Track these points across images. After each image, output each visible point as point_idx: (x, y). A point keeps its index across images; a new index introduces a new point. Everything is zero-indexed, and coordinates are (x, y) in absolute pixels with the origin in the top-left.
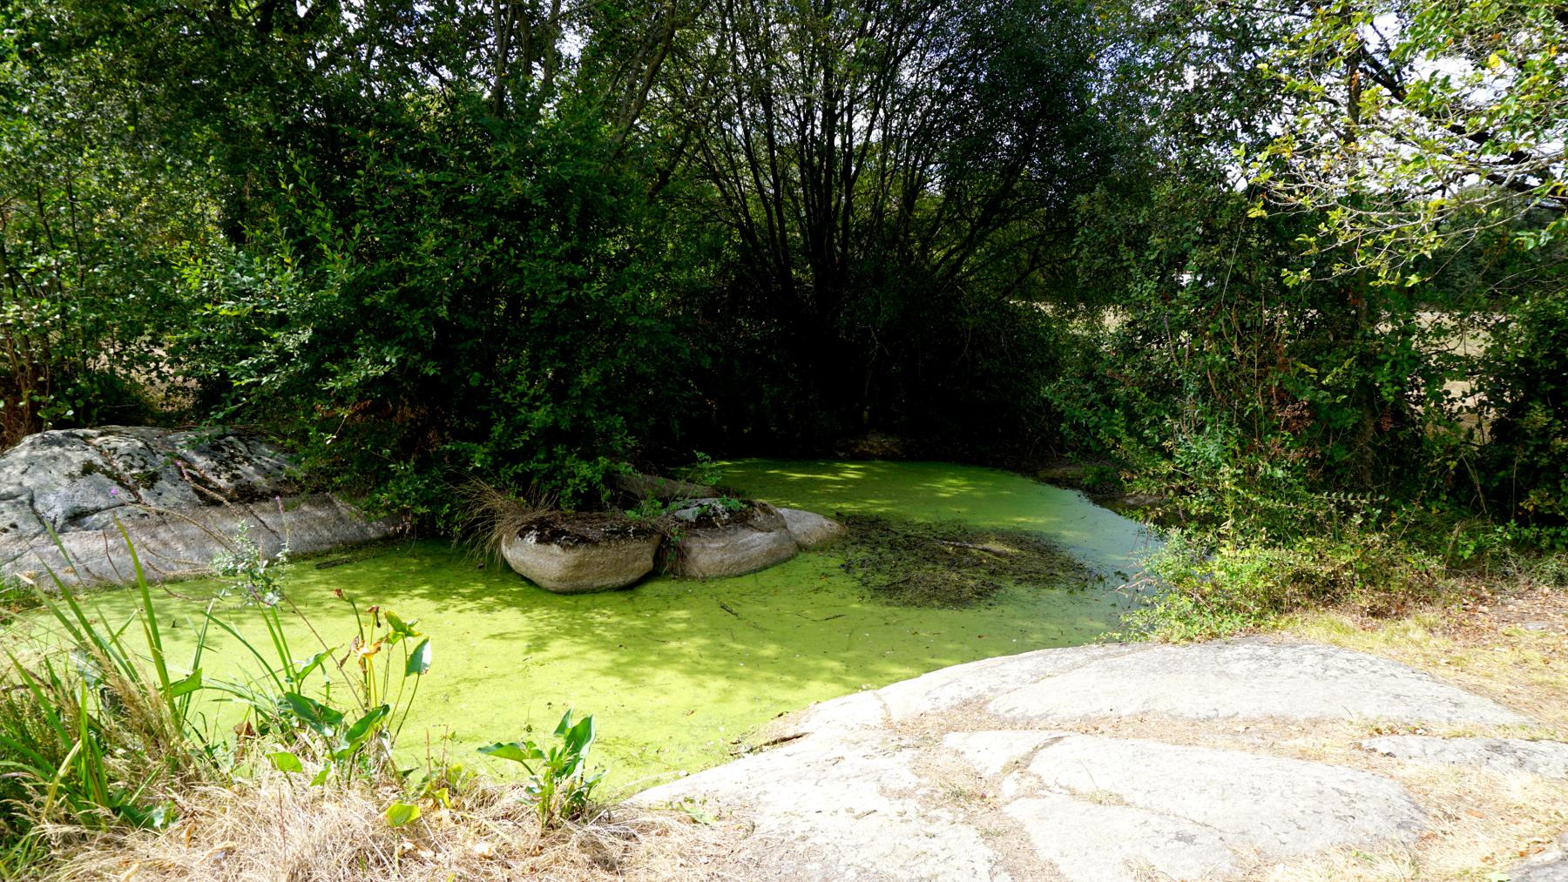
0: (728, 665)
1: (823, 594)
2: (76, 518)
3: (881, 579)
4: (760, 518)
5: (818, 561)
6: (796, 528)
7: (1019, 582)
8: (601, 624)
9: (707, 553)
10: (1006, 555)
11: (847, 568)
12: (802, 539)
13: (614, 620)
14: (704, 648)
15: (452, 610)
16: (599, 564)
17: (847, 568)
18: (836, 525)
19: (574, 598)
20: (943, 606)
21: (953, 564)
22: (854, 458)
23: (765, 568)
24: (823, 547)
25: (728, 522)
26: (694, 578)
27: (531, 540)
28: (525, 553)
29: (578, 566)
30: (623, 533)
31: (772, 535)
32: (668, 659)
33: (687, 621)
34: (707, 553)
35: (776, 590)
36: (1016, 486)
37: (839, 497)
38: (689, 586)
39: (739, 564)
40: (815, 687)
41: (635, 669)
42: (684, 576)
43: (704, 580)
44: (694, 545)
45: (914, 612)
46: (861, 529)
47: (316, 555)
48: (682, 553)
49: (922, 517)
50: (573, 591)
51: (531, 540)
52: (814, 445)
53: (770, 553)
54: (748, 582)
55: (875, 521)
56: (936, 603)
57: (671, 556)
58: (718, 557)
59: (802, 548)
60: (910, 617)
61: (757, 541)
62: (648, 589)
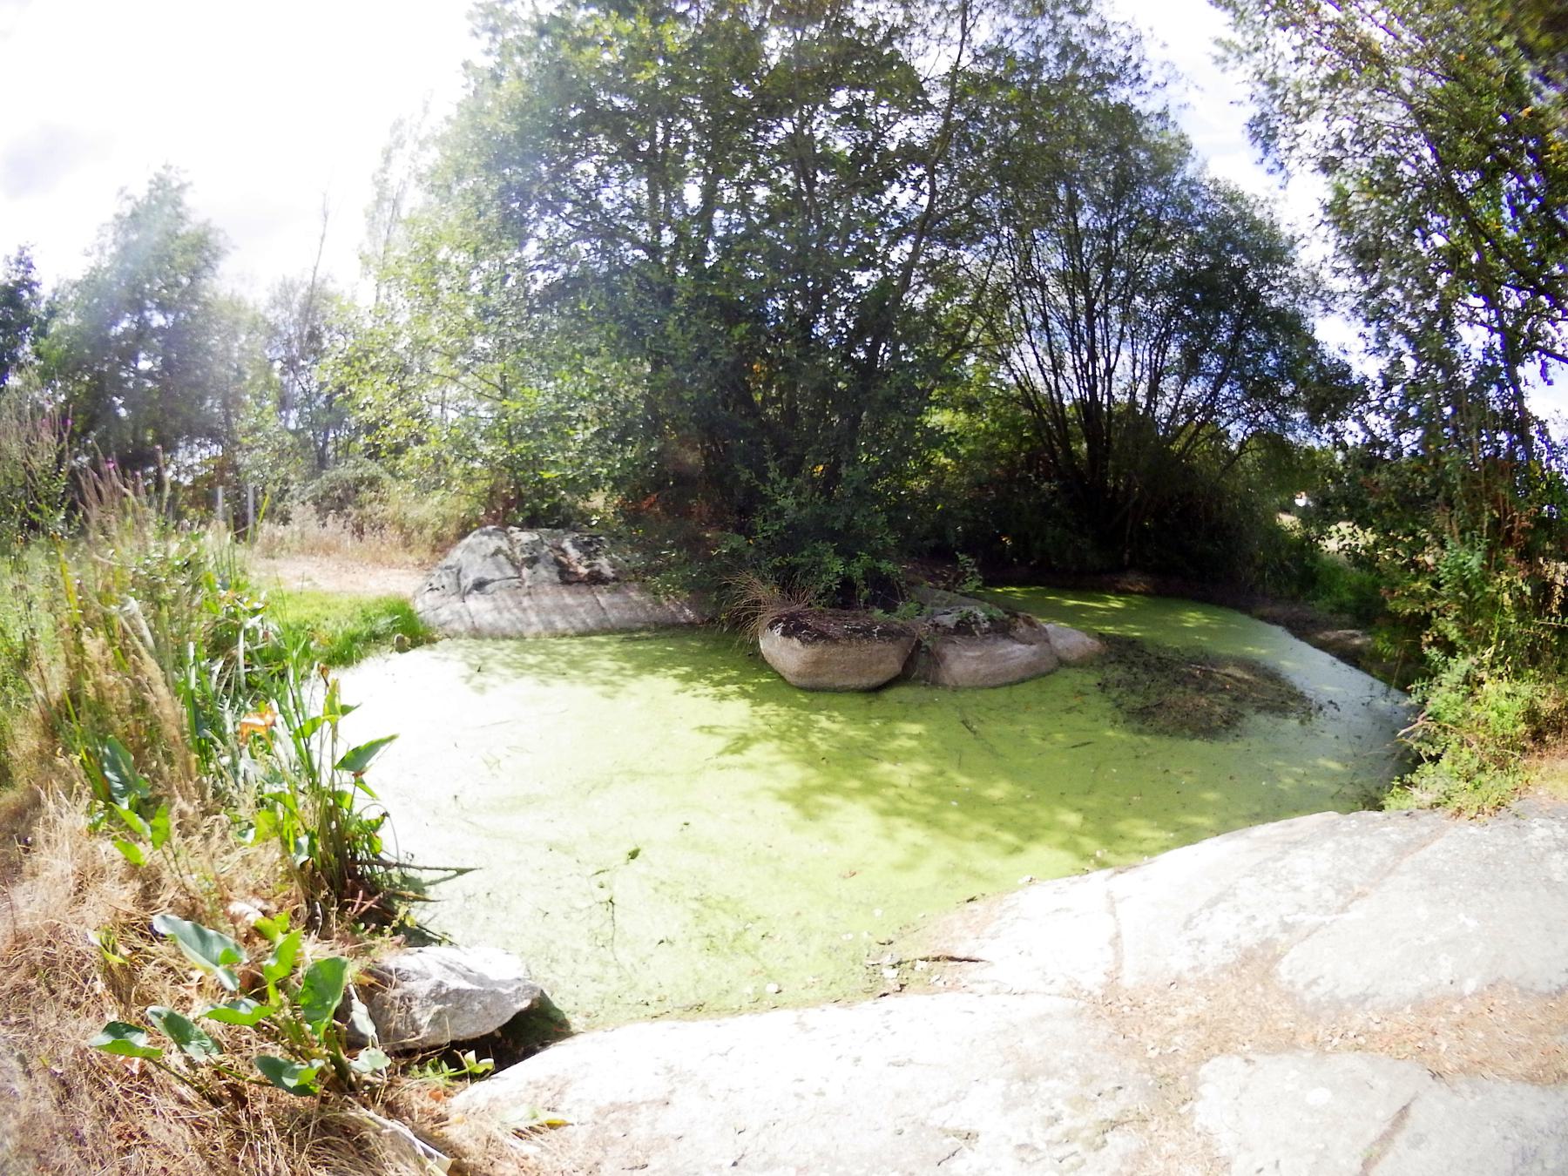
0: (935, 810)
1: (1075, 715)
2: (480, 585)
3: (1135, 701)
4: (1022, 629)
5: (1077, 678)
6: (1059, 644)
7: (1259, 710)
8: (822, 730)
9: (963, 661)
10: (1246, 681)
11: (1103, 687)
12: (1065, 655)
13: (835, 727)
14: (922, 777)
15: (690, 692)
16: (839, 663)
17: (1103, 687)
18: (1097, 643)
19: (812, 695)
20: (1194, 737)
21: (1201, 689)
22: (1119, 593)
23: (1022, 681)
24: (1083, 663)
25: (988, 631)
26: (945, 686)
27: (777, 632)
28: (778, 648)
29: (817, 663)
30: (867, 632)
31: (1034, 648)
32: (871, 787)
33: (918, 737)
34: (963, 661)
35: (1028, 707)
36: (1239, 621)
37: (1103, 621)
38: (938, 695)
39: (994, 675)
40: (1041, 854)
41: (822, 799)
42: (935, 683)
43: (956, 689)
44: (950, 652)
45: (1165, 743)
46: (1120, 651)
47: (630, 631)
48: (936, 659)
49: (1173, 642)
50: (814, 689)
51: (777, 632)
52: (1086, 579)
53: (1029, 666)
54: (1001, 696)
55: (1132, 642)
56: (1187, 731)
57: (922, 660)
58: (973, 666)
59: (1063, 663)
60: (1160, 746)
61: (1017, 653)
62: (891, 695)
